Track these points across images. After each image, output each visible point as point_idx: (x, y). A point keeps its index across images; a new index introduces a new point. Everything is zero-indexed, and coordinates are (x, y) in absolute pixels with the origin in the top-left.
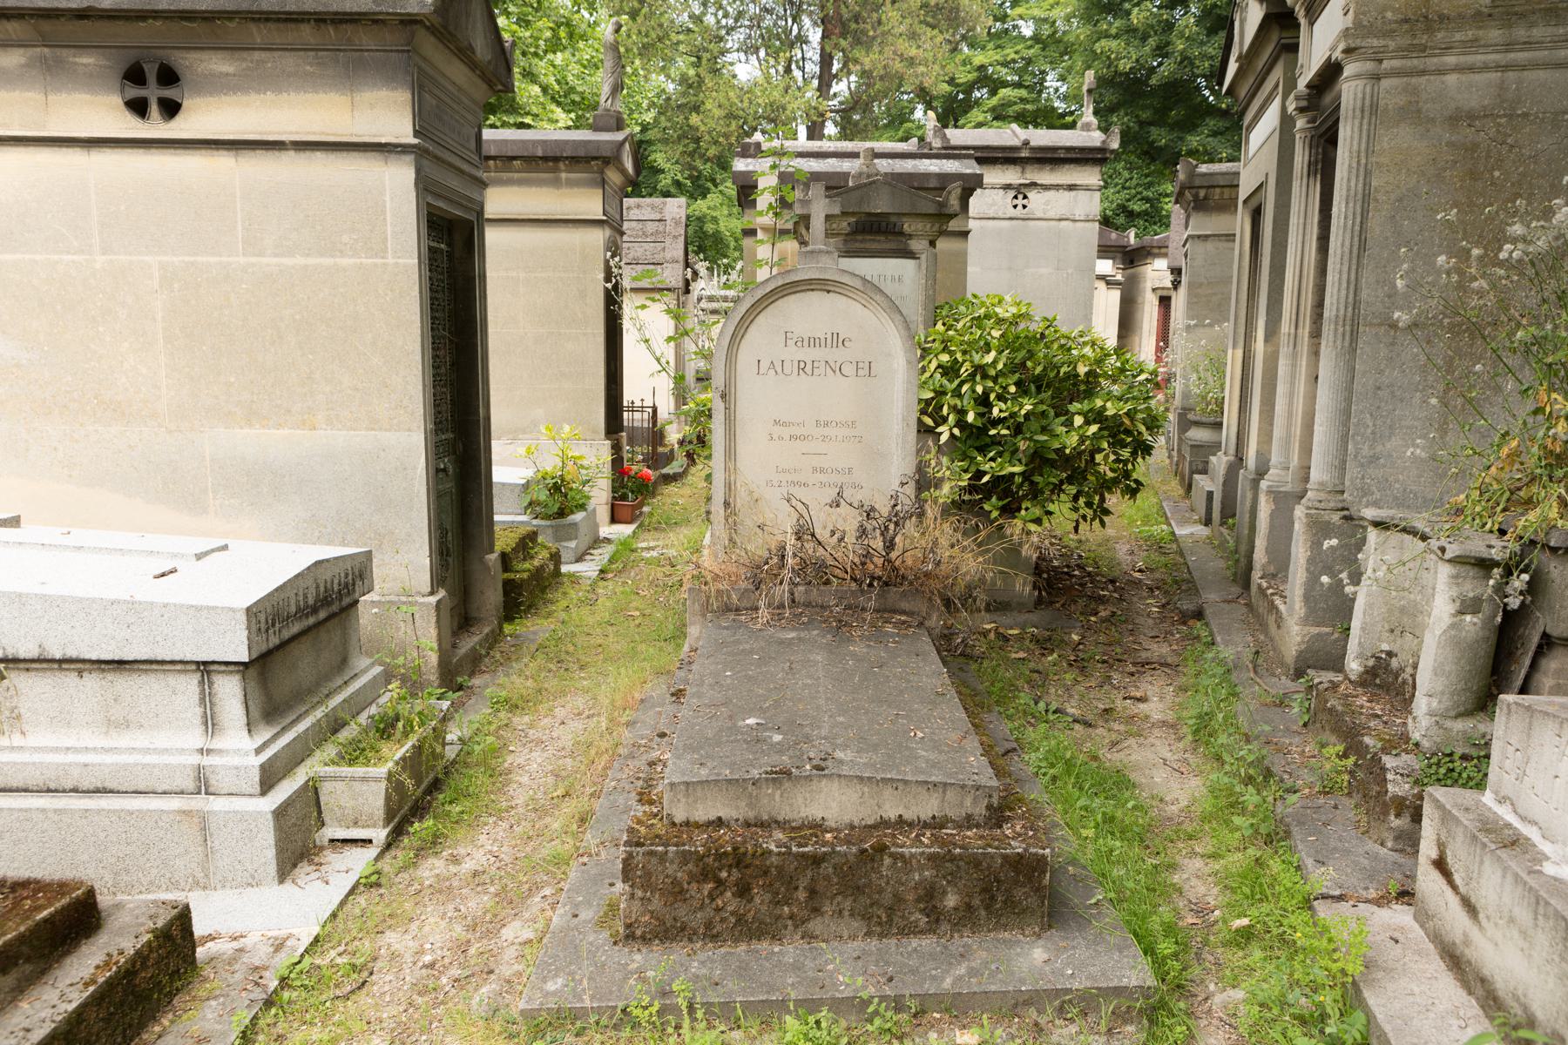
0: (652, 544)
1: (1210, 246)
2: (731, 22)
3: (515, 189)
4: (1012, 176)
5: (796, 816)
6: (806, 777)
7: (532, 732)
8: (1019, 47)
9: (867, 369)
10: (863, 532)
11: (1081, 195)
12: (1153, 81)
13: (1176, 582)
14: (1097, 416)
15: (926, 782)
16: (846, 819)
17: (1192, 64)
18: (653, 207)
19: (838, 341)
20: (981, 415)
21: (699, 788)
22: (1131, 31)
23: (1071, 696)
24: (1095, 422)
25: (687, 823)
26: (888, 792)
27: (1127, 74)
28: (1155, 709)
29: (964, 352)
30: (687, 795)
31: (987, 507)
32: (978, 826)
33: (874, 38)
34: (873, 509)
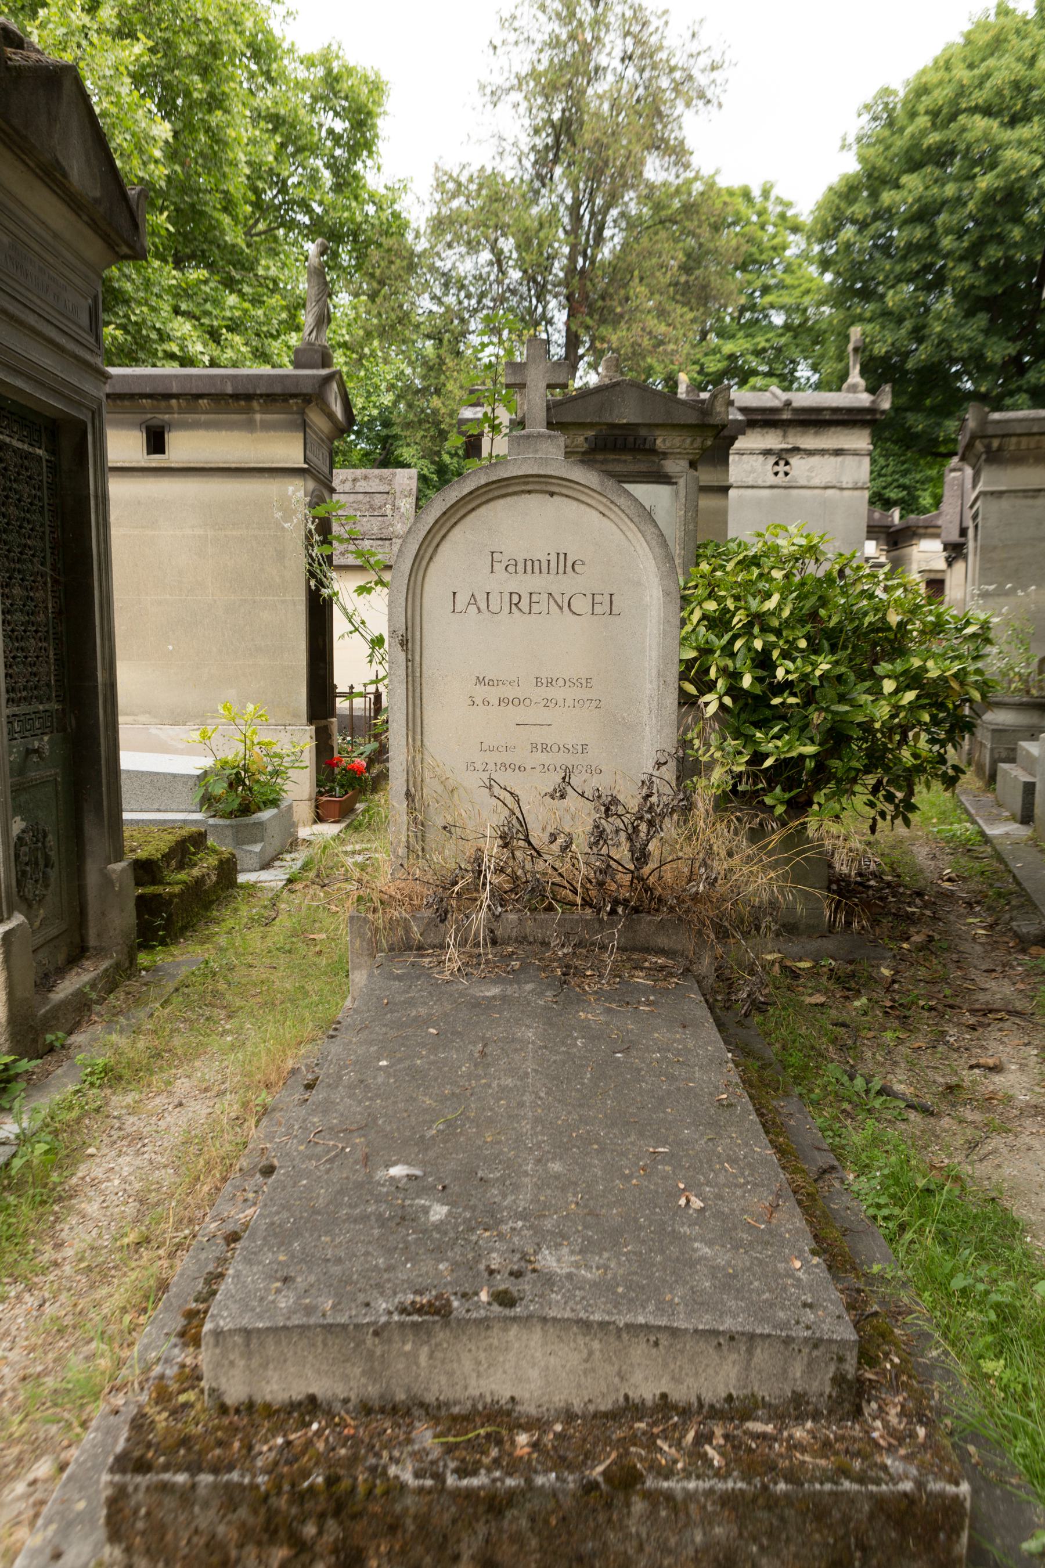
0: (358, 847)
1: (1005, 503)
2: (473, 302)
3: (201, 433)
4: (772, 440)
5: (459, 1393)
6: (478, 1322)
7: (132, 1119)
8: (769, 335)
9: (605, 605)
10: (599, 835)
11: (849, 460)
12: (910, 365)
13: (1000, 895)
14: (913, 679)
15: (715, 1333)
16: (559, 1400)
17: (949, 346)
18: (381, 479)
19: (565, 564)
20: (758, 680)
21: (270, 1341)
22: (886, 314)
23: (895, 1063)
24: (909, 688)
25: (250, 1407)
26: (639, 1351)
27: (882, 358)
28: (1016, 1082)
29: (737, 598)
30: (248, 1355)
31: (768, 801)
32: (816, 1416)
33: (621, 316)
34: (615, 801)
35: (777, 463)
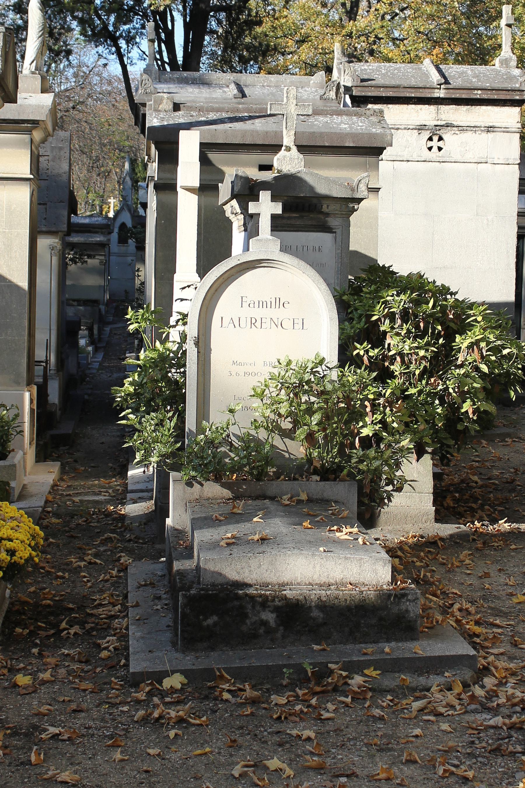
4: (426, 114)
11: (499, 136)
35: (430, 139)
